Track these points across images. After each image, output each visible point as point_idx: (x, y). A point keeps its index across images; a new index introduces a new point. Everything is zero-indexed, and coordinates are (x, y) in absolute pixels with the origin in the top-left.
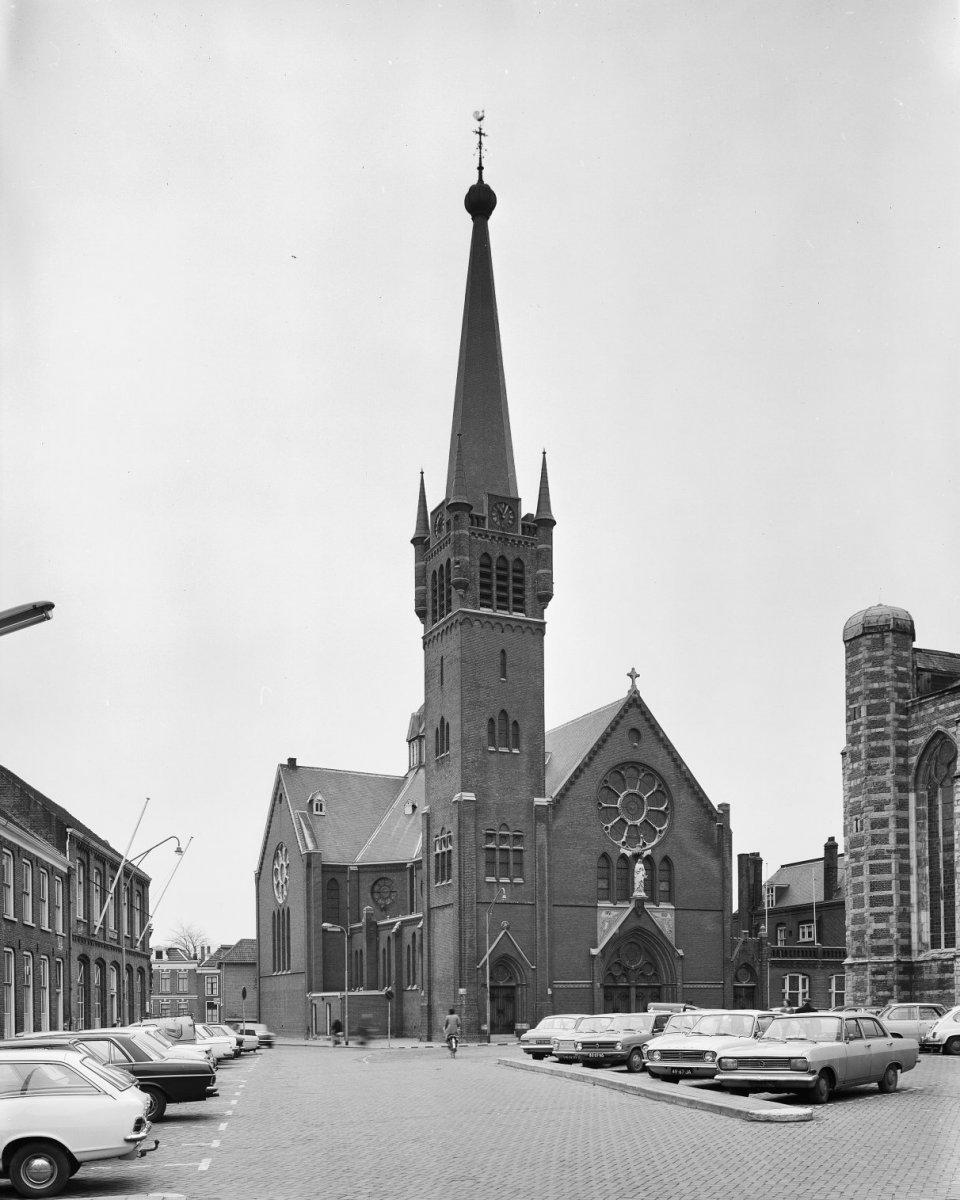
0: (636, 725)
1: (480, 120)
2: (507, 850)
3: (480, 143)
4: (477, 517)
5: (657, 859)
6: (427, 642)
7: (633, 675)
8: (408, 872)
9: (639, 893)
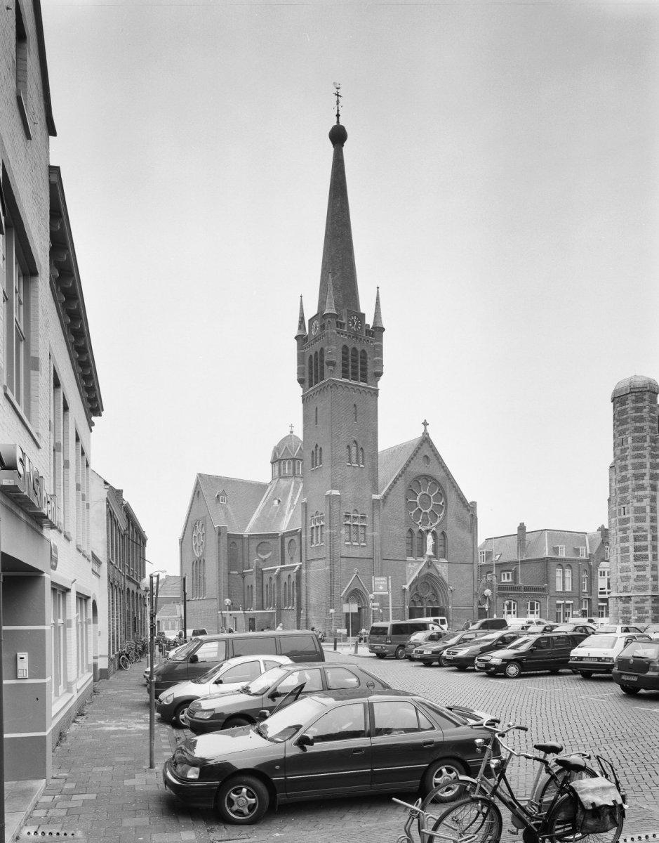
0: (427, 454)
1: (338, 89)
2: (357, 526)
3: (338, 101)
4: (340, 323)
6: (305, 399)
7: (425, 424)
8: (279, 539)
9: (429, 552)
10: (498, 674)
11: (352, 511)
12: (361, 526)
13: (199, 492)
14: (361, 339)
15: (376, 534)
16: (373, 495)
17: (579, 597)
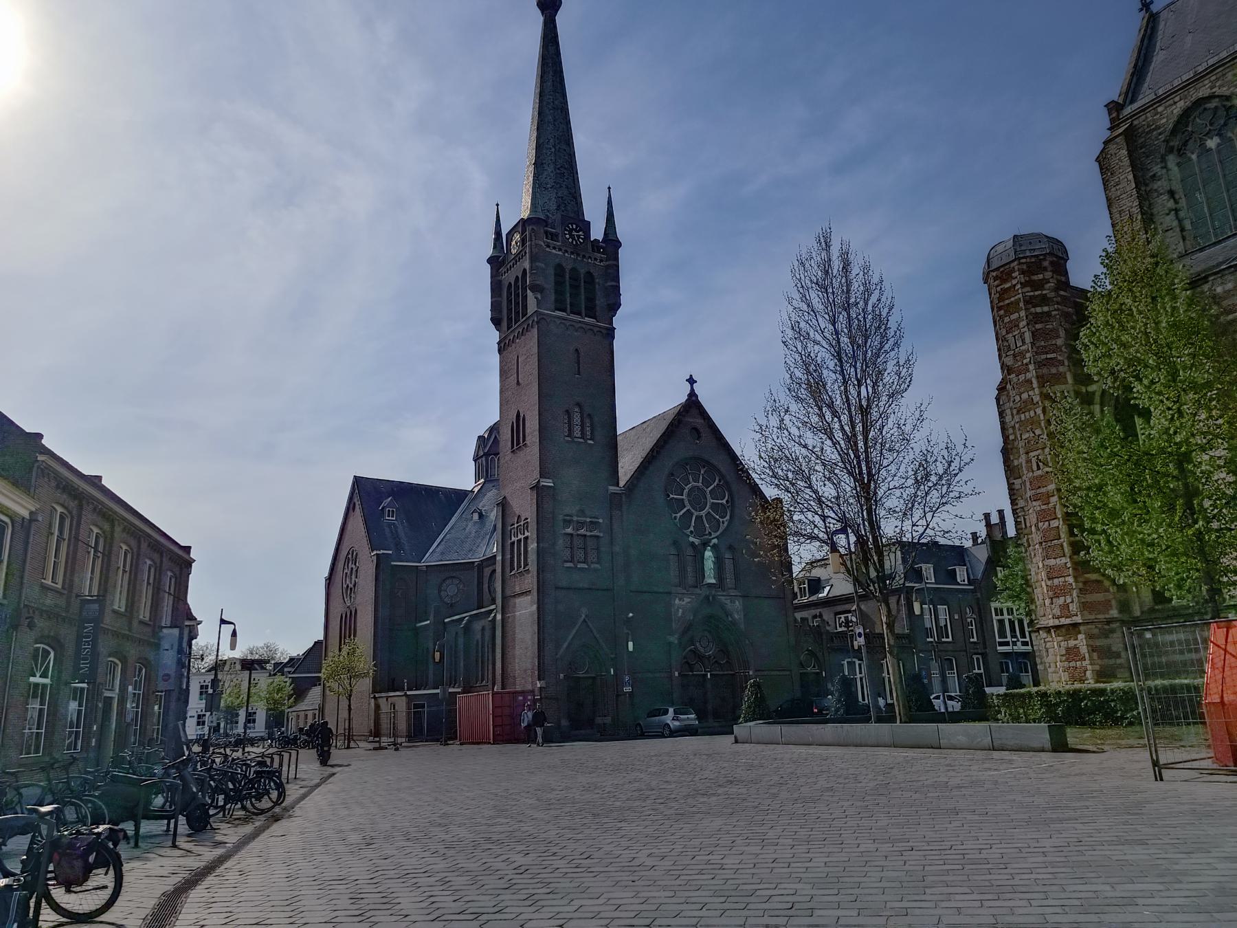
2: (585, 536)
4: (552, 234)
6: (502, 347)
7: (691, 381)
8: (476, 569)
10: (31, 915)
12: (591, 536)
16: (611, 488)
17: (966, 651)
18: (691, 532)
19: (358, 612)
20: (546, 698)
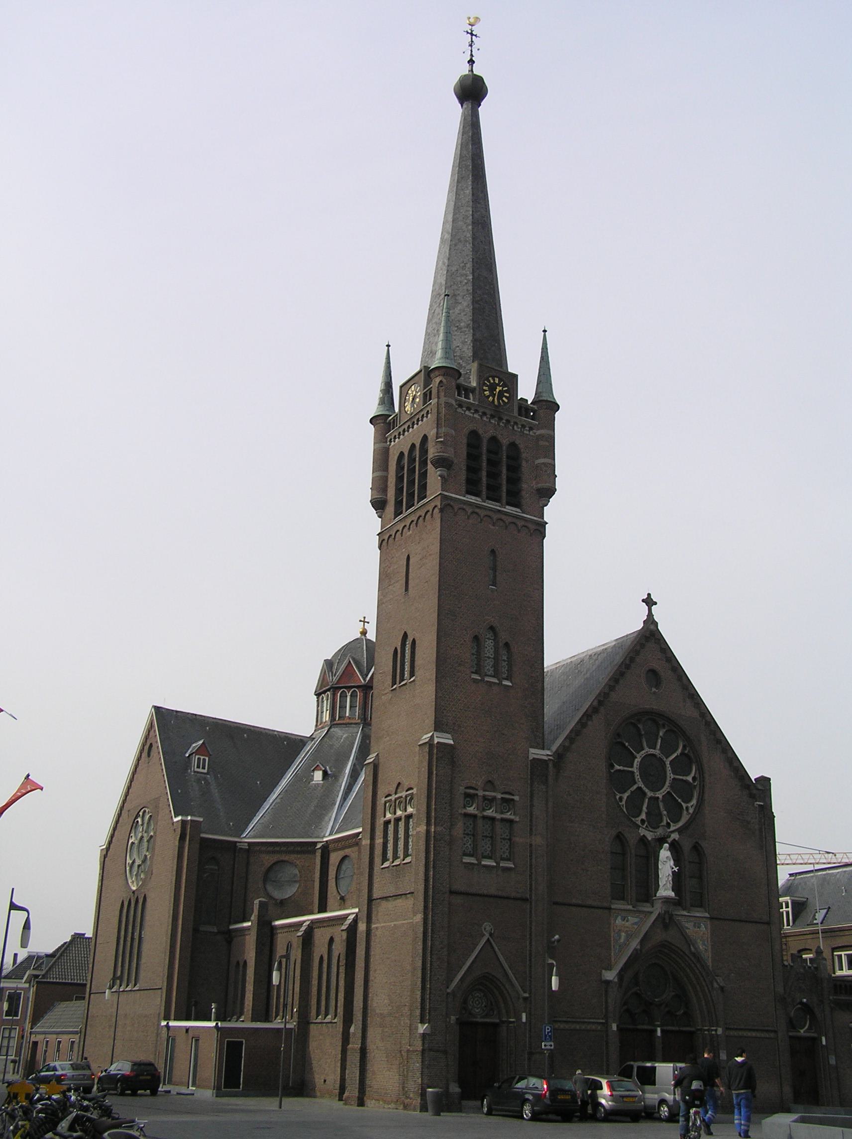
0: (655, 665)
2: (493, 819)
5: (687, 846)
6: (385, 541)
7: (649, 602)
8: (318, 854)
9: (665, 890)
11: (480, 783)
12: (503, 820)
13: (151, 745)
14: (508, 421)
15: (538, 840)
16: (532, 750)
18: (643, 821)
19: (148, 900)
20: (430, 1050)
